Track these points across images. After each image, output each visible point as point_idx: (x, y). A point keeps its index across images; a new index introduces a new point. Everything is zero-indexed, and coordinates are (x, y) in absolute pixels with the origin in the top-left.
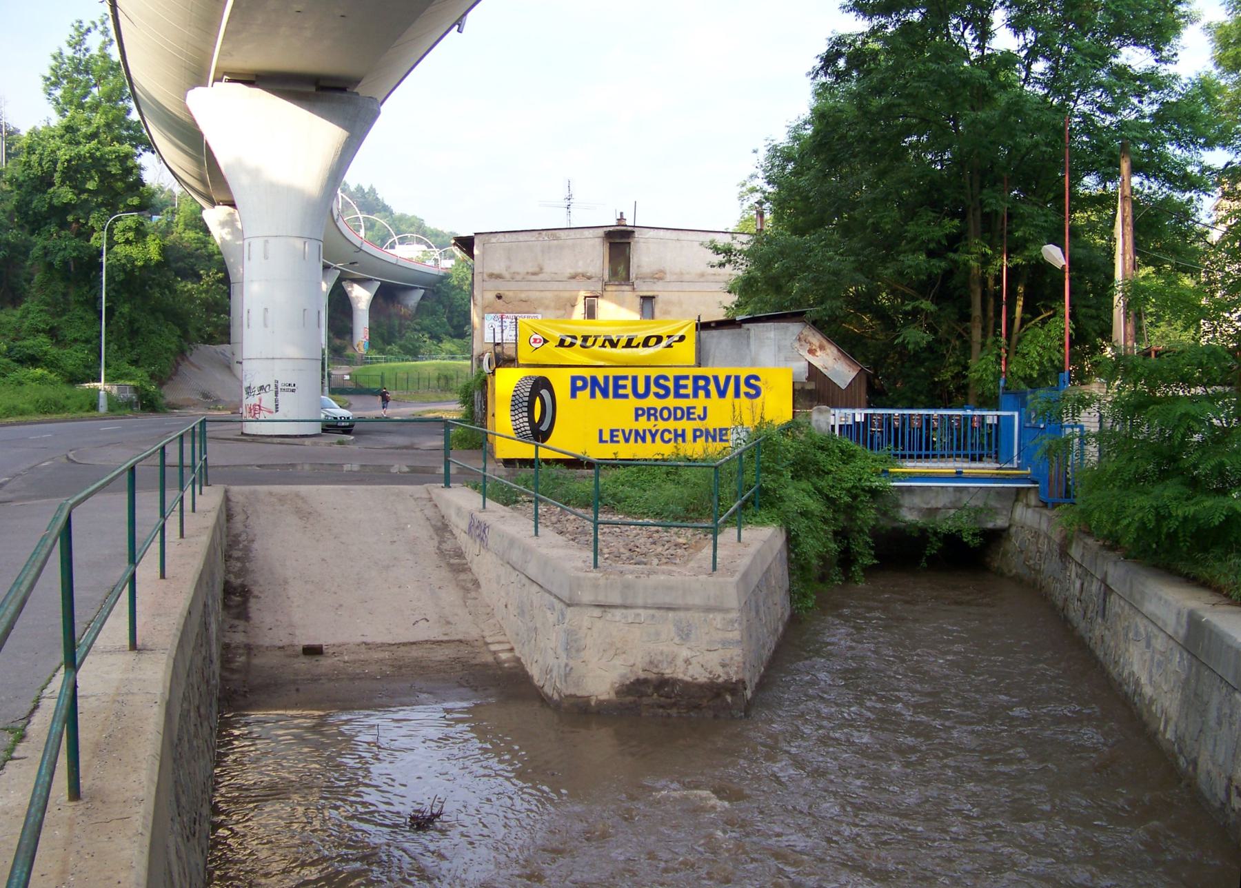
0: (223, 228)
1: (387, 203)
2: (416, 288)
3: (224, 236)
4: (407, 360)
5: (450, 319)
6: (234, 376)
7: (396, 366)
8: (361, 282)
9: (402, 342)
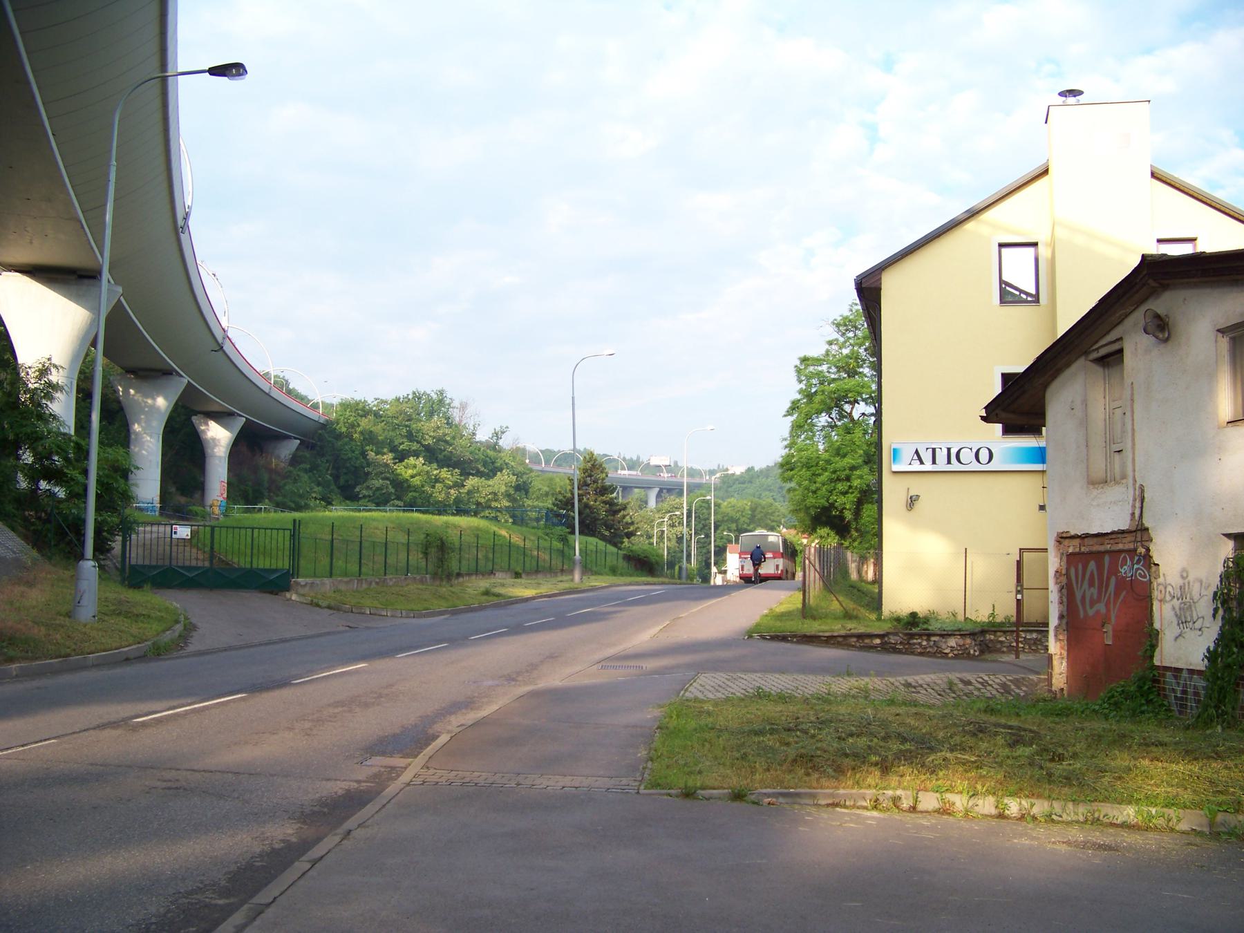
2: (288, 437)
4: (370, 510)
5: (336, 478)
8: (221, 417)
9: (279, 499)
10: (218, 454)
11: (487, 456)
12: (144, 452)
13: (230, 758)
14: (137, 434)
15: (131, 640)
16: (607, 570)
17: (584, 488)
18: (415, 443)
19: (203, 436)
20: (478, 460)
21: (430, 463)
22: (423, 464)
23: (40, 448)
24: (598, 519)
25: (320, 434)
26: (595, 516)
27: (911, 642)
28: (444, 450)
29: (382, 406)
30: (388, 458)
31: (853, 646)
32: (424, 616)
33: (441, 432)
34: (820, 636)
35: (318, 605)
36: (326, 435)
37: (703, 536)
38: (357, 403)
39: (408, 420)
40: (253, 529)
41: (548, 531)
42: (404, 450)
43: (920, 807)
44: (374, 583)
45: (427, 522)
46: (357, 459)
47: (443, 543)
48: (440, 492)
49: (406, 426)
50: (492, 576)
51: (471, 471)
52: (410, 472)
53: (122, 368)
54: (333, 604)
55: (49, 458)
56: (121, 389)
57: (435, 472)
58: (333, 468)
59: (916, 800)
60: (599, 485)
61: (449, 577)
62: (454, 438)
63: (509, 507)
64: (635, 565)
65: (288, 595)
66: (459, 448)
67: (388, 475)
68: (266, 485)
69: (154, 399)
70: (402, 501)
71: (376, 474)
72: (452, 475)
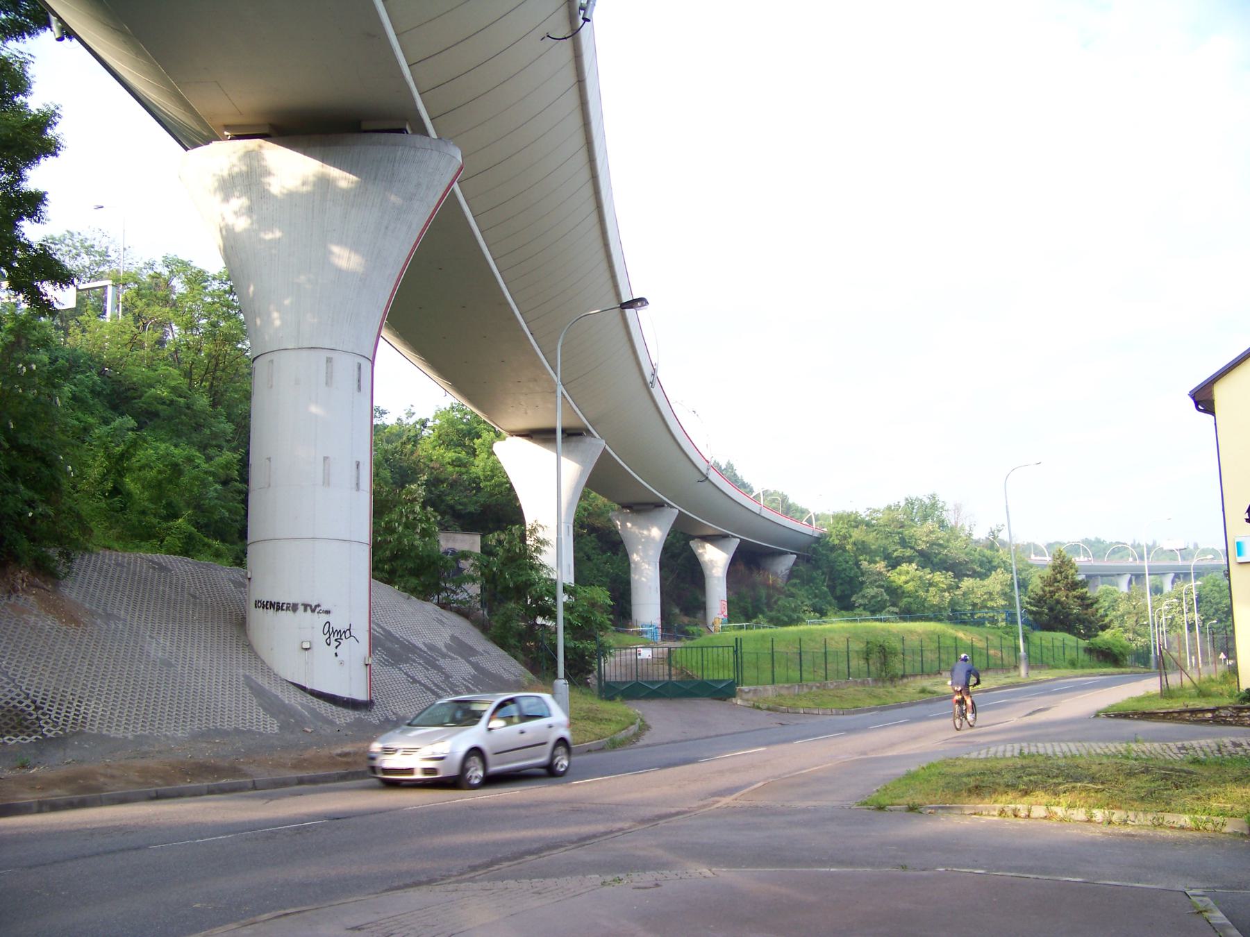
0: (226, 199)
1: (746, 480)
2: (786, 553)
3: (231, 220)
5: (832, 588)
6: (249, 647)
7: (757, 634)
8: (715, 539)
9: (773, 614)
10: (716, 575)
11: (984, 556)
12: (644, 579)
13: (618, 798)
14: (636, 563)
15: (593, 737)
16: (1066, 664)
17: (1056, 584)
18: (909, 549)
19: (701, 559)
20: (974, 561)
21: (923, 568)
22: (916, 570)
23: (534, 593)
24: (1072, 614)
25: (814, 548)
26: (1067, 612)
27: (1241, 714)
28: (939, 553)
29: (874, 515)
30: (881, 566)
31: (1187, 720)
32: (853, 713)
33: (933, 537)
34: (1157, 713)
35: (758, 708)
36: (820, 549)
37: (1215, 621)
38: (849, 516)
39: (900, 527)
40: (702, 647)
41: (1008, 630)
42: (898, 557)
43: (1033, 815)
44: (814, 688)
45: (883, 630)
46: (851, 569)
47: (913, 650)
48: (934, 596)
49: (899, 533)
50: (939, 675)
51: (968, 573)
52: (903, 578)
53: (619, 504)
54: (771, 706)
55: (541, 598)
56: (619, 523)
57: (928, 577)
58: (830, 579)
59: (1029, 811)
60: (1069, 581)
61: (893, 679)
62: (948, 541)
63: (1006, 605)
64: (1098, 657)
65: (734, 700)
66: (956, 551)
67: (882, 583)
68: (764, 600)
69: (649, 530)
70: (897, 607)
71: (871, 583)
72: (946, 578)
